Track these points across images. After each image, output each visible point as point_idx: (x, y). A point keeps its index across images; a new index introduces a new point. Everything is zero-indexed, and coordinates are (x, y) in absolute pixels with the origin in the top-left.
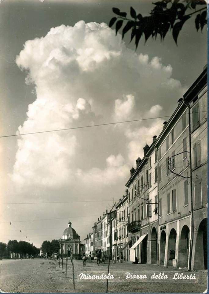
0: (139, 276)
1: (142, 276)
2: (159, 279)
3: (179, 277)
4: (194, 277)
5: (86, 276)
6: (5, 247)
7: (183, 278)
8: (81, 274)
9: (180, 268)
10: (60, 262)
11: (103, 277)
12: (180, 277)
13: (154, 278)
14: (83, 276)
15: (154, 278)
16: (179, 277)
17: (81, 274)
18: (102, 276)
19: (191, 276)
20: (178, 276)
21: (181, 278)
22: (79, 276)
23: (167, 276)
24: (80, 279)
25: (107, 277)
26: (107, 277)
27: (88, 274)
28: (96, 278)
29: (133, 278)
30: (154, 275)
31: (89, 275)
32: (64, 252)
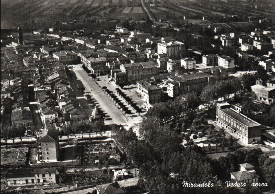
2: (209, 187)
5: (188, 184)
11: (204, 185)
14: (186, 184)
15: (203, 186)
19: (242, 183)
23: (213, 184)
25: (208, 185)
26: (208, 185)
28: (198, 186)
30: (203, 184)
31: (191, 184)
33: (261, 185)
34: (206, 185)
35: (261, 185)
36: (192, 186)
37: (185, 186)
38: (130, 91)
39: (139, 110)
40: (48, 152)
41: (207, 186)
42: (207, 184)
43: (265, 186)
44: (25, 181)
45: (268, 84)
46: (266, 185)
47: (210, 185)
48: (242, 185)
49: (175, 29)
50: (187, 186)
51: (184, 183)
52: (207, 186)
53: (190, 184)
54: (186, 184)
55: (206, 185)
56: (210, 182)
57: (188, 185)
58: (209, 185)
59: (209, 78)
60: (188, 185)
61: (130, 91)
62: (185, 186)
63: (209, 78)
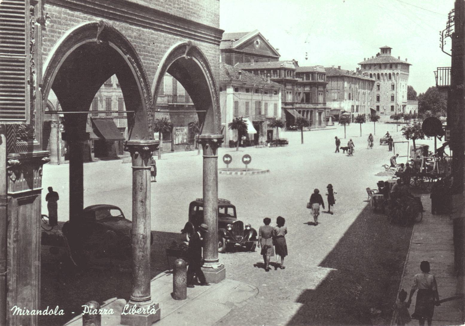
0: (107, 310)
1: (107, 310)
3: (131, 312)
4: (61, 312)
5: (21, 310)
6: (95, 156)
7: (138, 312)
8: (14, 307)
9: (458, 264)
10: (269, 319)
11: (48, 312)
12: (133, 310)
13: (47, 314)
14: (18, 310)
15: (46, 314)
16: (131, 312)
17: (14, 307)
18: (47, 310)
20: (129, 309)
21: (134, 312)
22: (12, 310)
23: (62, 311)
24: (13, 314)
25: (54, 312)
26: (54, 312)
27: (25, 308)
28: (37, 313)
29: (44, 314)
30: (47, 310)
32: (287, 71)
33: (30, 313)
34: (51, 313)
35: (30, 313)
36: (27, 314)
37: (17, 314)
38: (375, 134)
39: (280, 76)
40: (255, 174)
41: (53, 313)
42: (53, 311)
43: (59, 314)
44: (188, 294)
45: (327, 270)
46: (62, 314)
47: (58, 312)
48: (149, 311)
49: (412, 194)
50: (20, 314)
51: (15, 308)
52: (53, 313)
53: (24, 311)
54: (18, 310)
55: (51, 313)
56: (58, 307)
57: (22, 312)
58: (55, 312)
59: (311, 79)
60: (22, 312)
61: (375, 134)
62: (17, 314)
63: (311, 79)
